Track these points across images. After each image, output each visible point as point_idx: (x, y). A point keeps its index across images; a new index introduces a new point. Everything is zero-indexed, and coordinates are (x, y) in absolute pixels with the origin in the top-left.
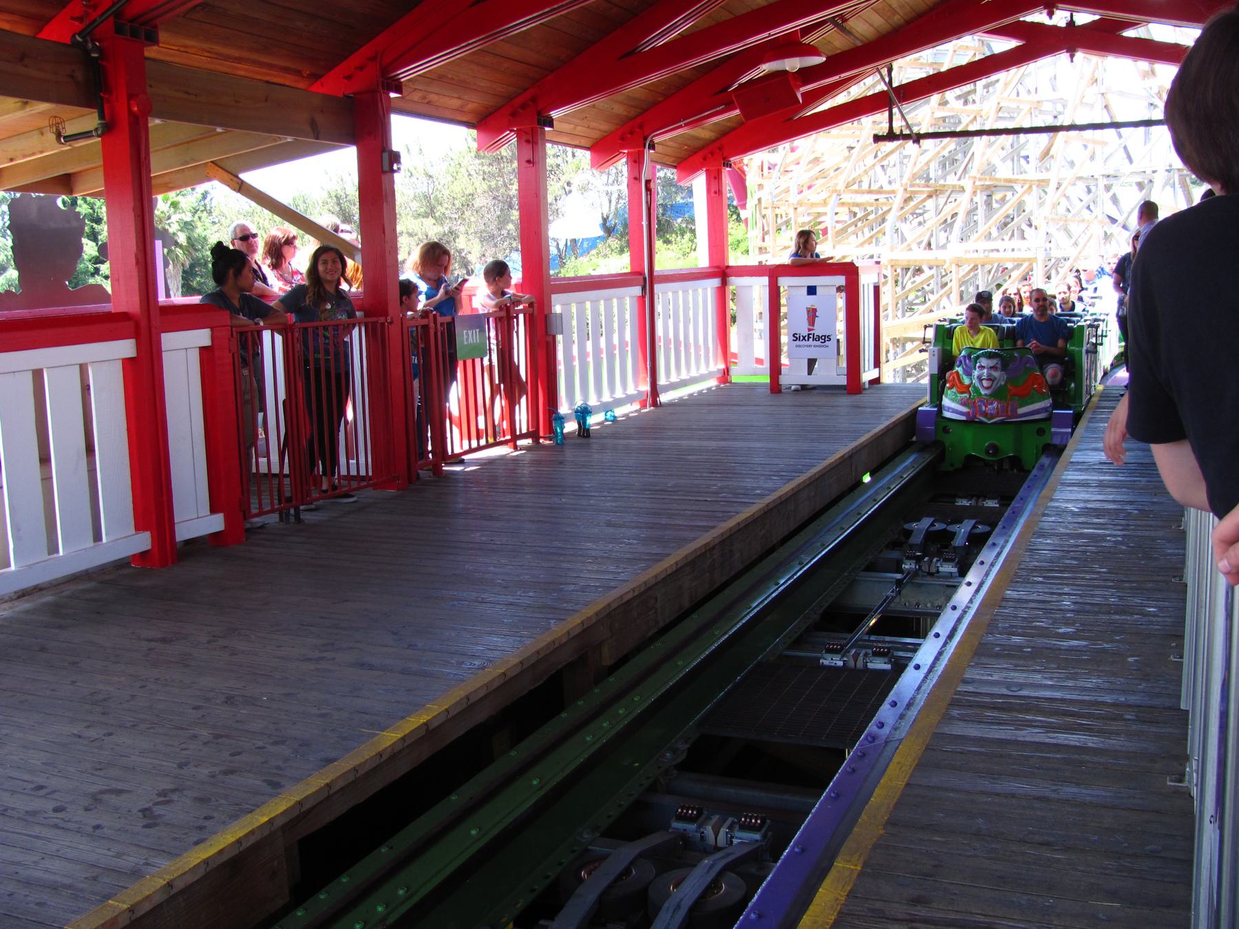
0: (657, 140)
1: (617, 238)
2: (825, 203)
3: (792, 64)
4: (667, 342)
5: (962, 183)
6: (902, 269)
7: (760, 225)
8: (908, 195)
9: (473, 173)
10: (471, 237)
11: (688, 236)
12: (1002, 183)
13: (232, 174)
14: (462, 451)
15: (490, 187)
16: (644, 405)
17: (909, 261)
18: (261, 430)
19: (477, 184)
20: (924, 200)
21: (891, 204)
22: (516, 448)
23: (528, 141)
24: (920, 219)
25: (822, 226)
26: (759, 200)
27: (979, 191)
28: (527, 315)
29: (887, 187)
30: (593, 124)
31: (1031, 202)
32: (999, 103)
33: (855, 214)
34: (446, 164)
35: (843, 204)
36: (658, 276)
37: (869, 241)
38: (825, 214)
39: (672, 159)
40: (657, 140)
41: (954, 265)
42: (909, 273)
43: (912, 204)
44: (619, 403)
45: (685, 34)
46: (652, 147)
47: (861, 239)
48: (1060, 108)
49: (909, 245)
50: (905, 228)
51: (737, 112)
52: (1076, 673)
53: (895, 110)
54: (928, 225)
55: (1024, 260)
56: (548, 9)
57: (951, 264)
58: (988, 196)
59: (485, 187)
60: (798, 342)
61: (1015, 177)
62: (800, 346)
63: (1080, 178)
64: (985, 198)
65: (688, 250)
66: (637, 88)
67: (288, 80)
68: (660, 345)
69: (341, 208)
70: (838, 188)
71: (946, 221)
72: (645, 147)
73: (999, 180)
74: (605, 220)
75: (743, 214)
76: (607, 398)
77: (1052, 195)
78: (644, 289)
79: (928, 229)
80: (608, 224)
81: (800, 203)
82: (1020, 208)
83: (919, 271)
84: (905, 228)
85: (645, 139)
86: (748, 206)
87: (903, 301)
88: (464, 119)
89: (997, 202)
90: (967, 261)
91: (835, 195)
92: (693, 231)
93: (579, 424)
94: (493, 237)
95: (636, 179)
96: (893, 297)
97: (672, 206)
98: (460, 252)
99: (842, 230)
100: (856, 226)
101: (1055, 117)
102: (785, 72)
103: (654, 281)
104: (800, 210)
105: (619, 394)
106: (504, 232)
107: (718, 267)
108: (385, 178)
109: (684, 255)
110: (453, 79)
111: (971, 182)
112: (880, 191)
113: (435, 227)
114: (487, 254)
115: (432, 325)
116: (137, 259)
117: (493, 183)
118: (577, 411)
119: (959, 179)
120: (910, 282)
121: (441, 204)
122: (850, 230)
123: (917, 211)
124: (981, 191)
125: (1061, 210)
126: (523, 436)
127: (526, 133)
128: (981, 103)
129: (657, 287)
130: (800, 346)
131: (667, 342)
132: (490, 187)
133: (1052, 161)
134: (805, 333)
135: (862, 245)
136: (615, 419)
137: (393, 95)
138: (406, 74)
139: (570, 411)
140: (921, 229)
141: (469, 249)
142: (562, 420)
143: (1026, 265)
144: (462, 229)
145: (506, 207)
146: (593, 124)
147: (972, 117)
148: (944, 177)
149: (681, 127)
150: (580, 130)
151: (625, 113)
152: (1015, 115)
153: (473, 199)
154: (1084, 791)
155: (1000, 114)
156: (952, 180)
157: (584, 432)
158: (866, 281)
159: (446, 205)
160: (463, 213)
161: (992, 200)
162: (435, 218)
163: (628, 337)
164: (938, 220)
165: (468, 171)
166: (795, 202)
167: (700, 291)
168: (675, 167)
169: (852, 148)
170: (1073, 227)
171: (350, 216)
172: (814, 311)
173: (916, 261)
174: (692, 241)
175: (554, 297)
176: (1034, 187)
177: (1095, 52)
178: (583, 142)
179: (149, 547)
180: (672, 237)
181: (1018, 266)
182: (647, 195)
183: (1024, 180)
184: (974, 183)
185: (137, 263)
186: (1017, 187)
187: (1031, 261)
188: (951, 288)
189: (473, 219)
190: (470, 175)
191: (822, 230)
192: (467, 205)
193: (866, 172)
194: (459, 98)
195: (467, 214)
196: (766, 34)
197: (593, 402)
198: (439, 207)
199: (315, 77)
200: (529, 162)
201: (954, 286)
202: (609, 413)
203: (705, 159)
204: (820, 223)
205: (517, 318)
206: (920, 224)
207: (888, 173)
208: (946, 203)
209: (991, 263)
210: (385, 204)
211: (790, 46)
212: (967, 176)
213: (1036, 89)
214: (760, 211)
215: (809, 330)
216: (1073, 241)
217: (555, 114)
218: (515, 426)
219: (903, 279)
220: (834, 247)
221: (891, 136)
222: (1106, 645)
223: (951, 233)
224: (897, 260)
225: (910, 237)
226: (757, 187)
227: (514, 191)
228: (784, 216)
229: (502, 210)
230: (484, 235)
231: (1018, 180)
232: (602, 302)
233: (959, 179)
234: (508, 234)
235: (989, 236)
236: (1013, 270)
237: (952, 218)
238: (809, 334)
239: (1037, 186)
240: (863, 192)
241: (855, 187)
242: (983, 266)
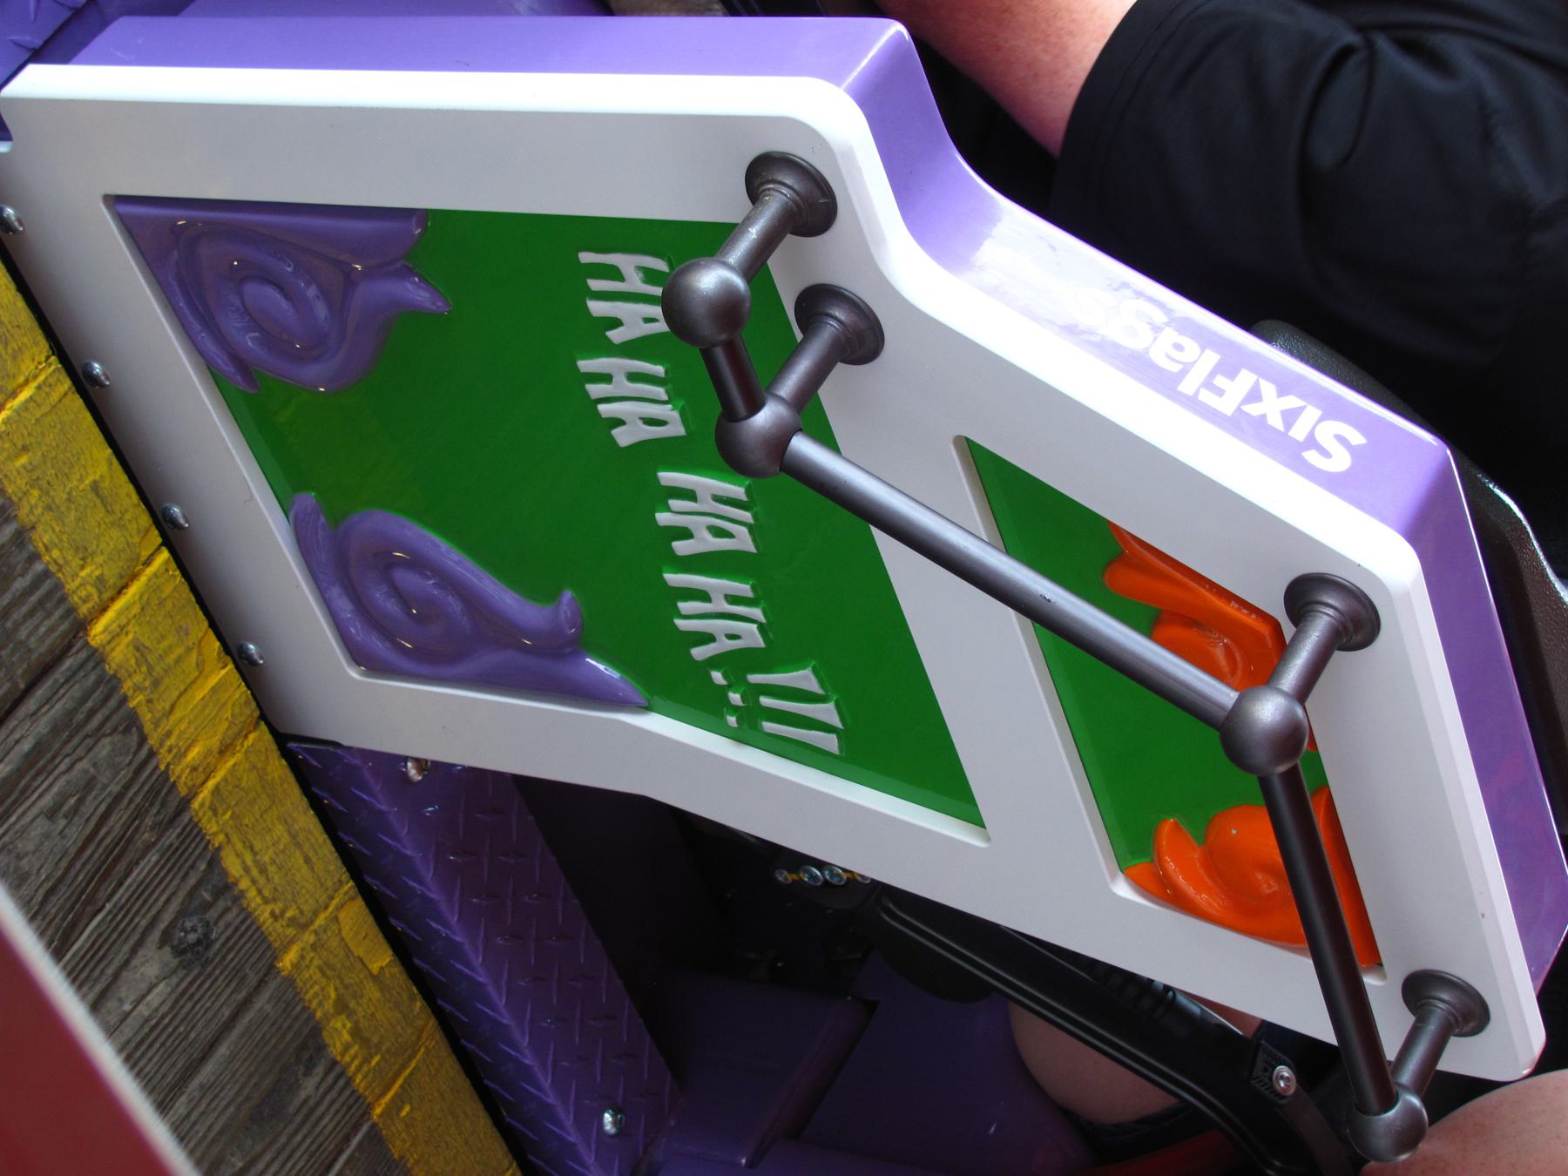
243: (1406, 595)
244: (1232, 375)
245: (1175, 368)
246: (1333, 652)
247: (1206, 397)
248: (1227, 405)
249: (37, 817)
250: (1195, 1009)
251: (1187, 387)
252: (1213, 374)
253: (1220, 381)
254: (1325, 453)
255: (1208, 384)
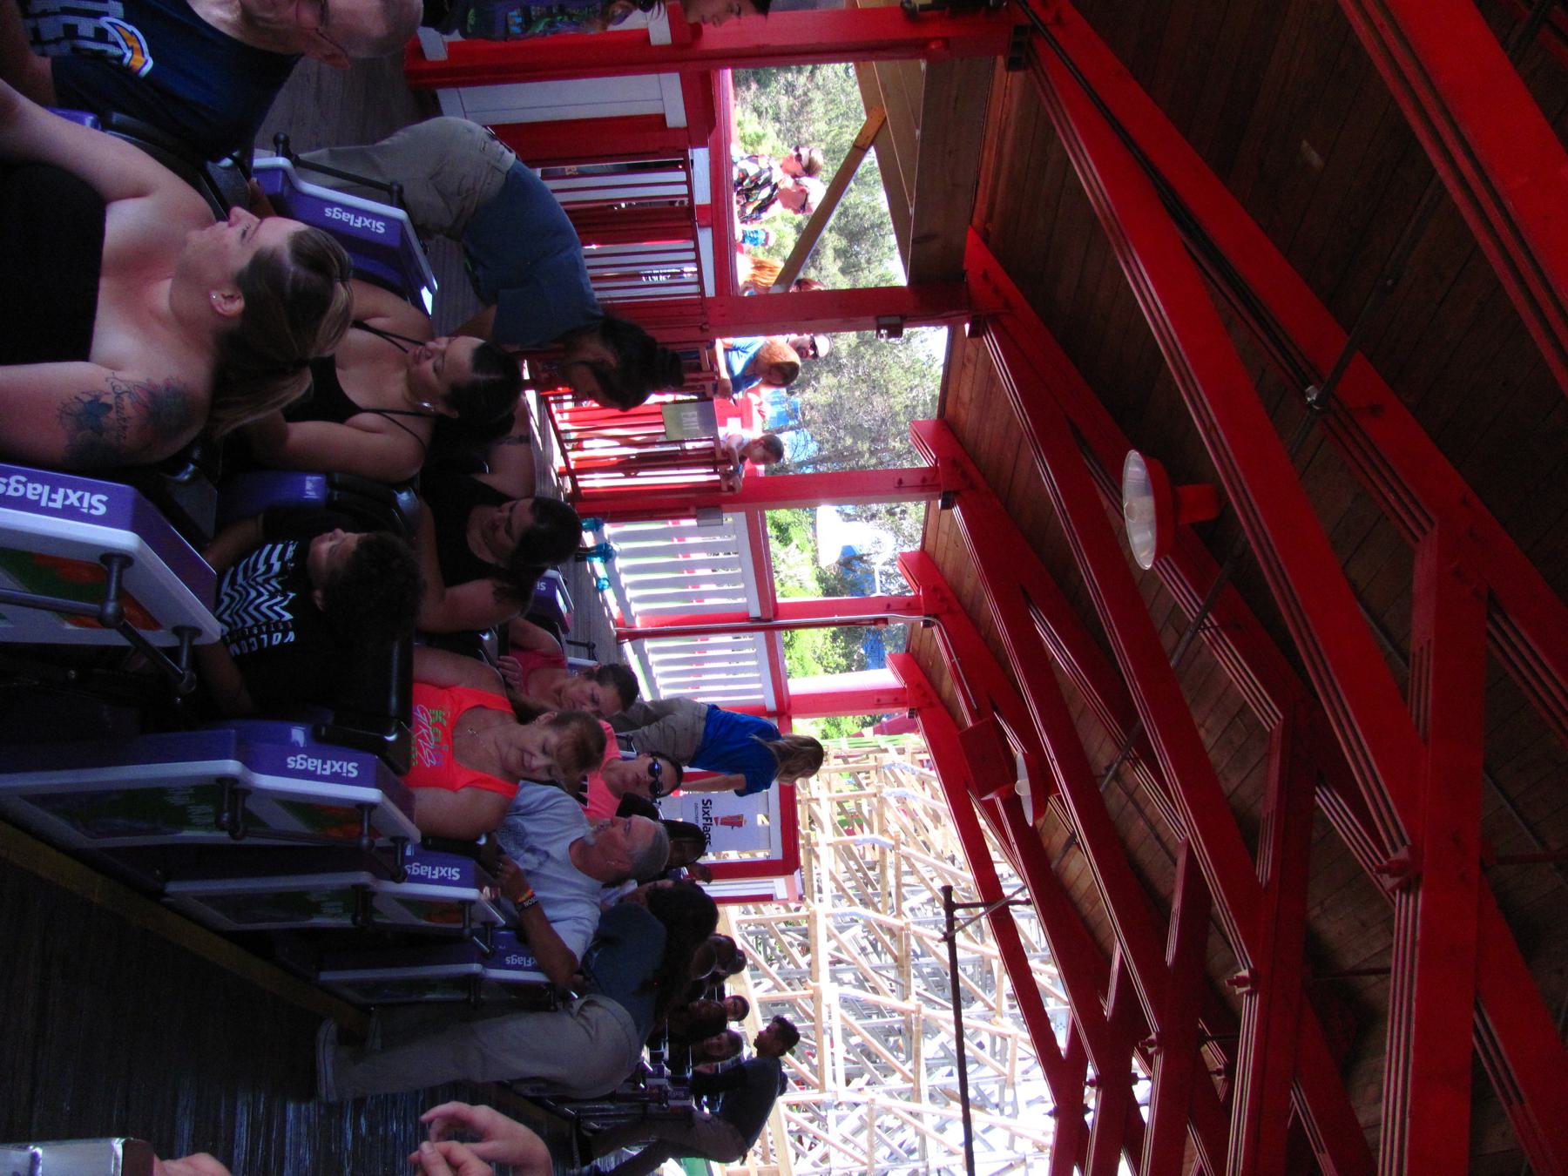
0: (935, 629)
1: (838, 574)
2: (883, 831)
3: (1023, 787)
4: (702, 649)
5: (913, 998)
6: (806, 929)
7: (855, 751)
8: (896, 933)
9: (914, 393)
10: (835, 392)
11: (843, 662)
12: (914, 1046)
13: (875, 137)
14: (557, 421)
15: (897, 414)
16: (617, 624)
17: (816, 937)
18: (574, 168)
19: (900, 399)
20: (892, 953)
21: (885, 912)
22: (561, 475)
23: (924, 480)
24: (870, 949)
25: (857, 829)
26: (885, 751)
27: (903, 1018)
28: (718, 484)
29: (905, 906)
30: (950, 555)
31: (895, 1082)
32: (1010, 1036)
33: (873, 869)
34: (925, 359)
35: (883, 853)
36: (773, 636)
37: (840, 888)
38: (872, 831)
39: (917, 649)
40: (935, 629)
41: (811, 992)
42: (801, 938)
43: (887, 938)
44: (620, 594)
45: (1053, 665)
46: (927, 624)
47: (840, 878)
48: (1008, 1110)
49: (835, 936)
50: (857, 930)
51: (970, 723)
52: (315, 1137)
53: (981, 910)
54: (862, 959)
55: (822, 1078)
56: (1065, 507)
57: (815, 989)
58: (900, 1031)
59: (897, 408)
60: (701, 806)
61: (923, 1062)
62: (696, 807)
63: (923, 1140)
64: (896, 1026)
65: (825, 663)
66: (991, 608)
67: (981, 206)
68: (698, 641)
69: (868, 229)
70: (902, 847)
71: (867, 980)
72: (926, 615)
73: (918, 1042)
74: (860, 558)
75: (868, 731)
76: (625, 579)
77: (900, 1105)
78: (758, 619)
79: (855, 959)
80: (855, 562)
81: (882, 801)
82: (888, 1070)
83: (806, 949)
84: (857, 930)
85: (936, 616)
86: (878, 736)
87: (767, 932)
88: (948, 405)
89: (896, 1042)
90: (818, 1009)
91: (893, 843)
92: (849, 669)
93: (592, 548)
94: (835, 419)
95: (889, 606)
96: (772, 919)
97: (880, 642)
98: (817, 378)
99: (852, 853)
100: (857, 871)
101: (997, 1106)
102: (1015, 778)
103: (768, 632)
104: (874, 800)
105: (630, 594)
106: (842, 433)
107: (789, 705)
108: (871, 320)
109: (819, 658)
110: (991, 394)
111: (913, 1008)
112: (901, 898)
113: (845, 347)
114: (814, 413)
115: (701, 375)
116: (763, 46)
117: (902, 418)
118: (607, 545)
119: (917, 994)
120: (792, 940)
121: (875, 353)
122: (852, 863)
123: (879, 945)
124: (903, 1021)
125: (889, 1121)
126: (574, 482)
127: (934, 478)
128: (1010, 1015)
129: (761, 635)
130: (696, 807)
131: (702, 649)
132: (897, 414)
133: (943, 1105)
134: (712, 815)
135: (833, 878)
136: (599, 590)
137: (967, 327)
138: (990, 343)
139: (606, 537)
140: (855, 950)
141: (820, 390)
142: (596, 528)
143: (817, 1081)
144: (845, 380)
145: (873, 435)
146: (950, 555)
147: (994, 1005)
148: (921, 975)
149: (951, 657)
150: (943, 538)
151: (965, 592)
152: (998, 1058)
153: (882, 394)
154: (185, 1144)
155: (998, 1040)
156: (917, 985)
157: (588, 553)
158: (778, 886)
159: (873, 359)
160: (864, 381)
161: (896, 1035)
162: (857, 346)
163: (708, 602)
164: (866, 970)
165: (916, 386)
166: (883, 795)
167: (757, 686)
168: (907, 651)
169: (953, 862)
170: (862, 1140)
171: (858, 241)
172: (740, 824)
173: (816, 945)
174: (838, 666)
175: (742, 515)
176: (911, 1085)
177: (79, 540)
178: (930, 542)
179: (427, 57)
180: (840, 643)
181: (814, 1069)
182: (870, 620)
183: (919, 1073)
184: (913, 1012)
185: (759, 47)
186: (910, 1065)
187: (821, 1087)
188: (784, 990)
189: (857, 393)
190: (912, 389)
191: (853, 830)
192: (875, 387)
193: (923, 880)
194: (971, 399)
195: (864, 387)
196: (1053, 756)
197: (619, 563)
198: (871, 351)
199: (985, 236)
200: (900, 482)
201: (789, 993)
202: (606, 583)
203: (918, 686)
204: (861, 827)
205: (715, 473)
206: (863, 949)
207: (926, 907)
208: (888, 979)
209: (819, 1040)
210: (840, 320)
211: (1043, 787)
212: (921, 1002)
213: (1028, 1080)
214: (872, 752)
215: (716, 819)
216: (850, 1137)
217: (956, 511)
218: (587, 473)
219: (794, 931)
220: (829, 845)
221: (950, 907)
222: (348, 1170)
223: (854, 987)
224: (815, 922)
225: (845, 937)
226: (901, 746)
227: (893, 444)
228: (868, 781)
229: (870, 429)
230: (838, 408)
231: (919, 1064)
232: (739, 570)
233: (917, 994)
234: (840, 438)
235: (847, 1033)
236: (810, 1064)
237: (872, 988)
238: (711, 819)
239: (912, 1089)
240: (898, 877)
241: (905, 868)
242: (814, 1028)
243: (139, 552)
244: (56, 492)
245: (37, 498)
246: (675, 71)
247: (51, 504)
248: (58, 505)
249: (1176, 648)
250: (1023, 941)
251: (43, 503)
252: (50, 495)
253: (53, 496)
254: (97, 509)
255: (50, 499)
